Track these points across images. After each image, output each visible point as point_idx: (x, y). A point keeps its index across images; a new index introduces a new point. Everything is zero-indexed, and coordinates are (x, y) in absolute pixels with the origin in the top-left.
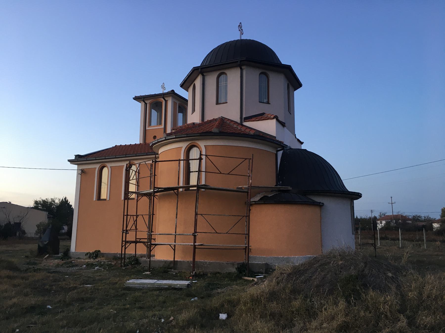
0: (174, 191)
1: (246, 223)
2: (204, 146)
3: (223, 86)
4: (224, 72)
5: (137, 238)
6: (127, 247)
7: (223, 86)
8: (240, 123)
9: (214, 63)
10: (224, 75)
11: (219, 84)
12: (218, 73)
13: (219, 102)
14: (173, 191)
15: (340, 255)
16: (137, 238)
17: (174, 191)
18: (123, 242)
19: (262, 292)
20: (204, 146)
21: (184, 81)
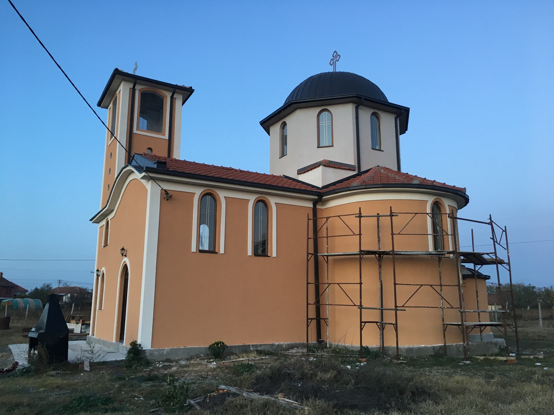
0: (376, 255)
1: (473, 311)
2: (275, 203)
3: (325, 125)
4: (327, 108)
5: (309, 317)
6: (483, 330)
7: (325, 125)
8: (361, 171)
9: (300, 98)
10: (326, 112)
11: (320, 125)
12: (318, 110)
13: (321, 145)
14: (374, 255)
15: (199, 370)
16: (309, 317)
17: (376, 255)
18: (309, 320)
19: (107, 404)
20: (275, 203)
21: (263, 122)
